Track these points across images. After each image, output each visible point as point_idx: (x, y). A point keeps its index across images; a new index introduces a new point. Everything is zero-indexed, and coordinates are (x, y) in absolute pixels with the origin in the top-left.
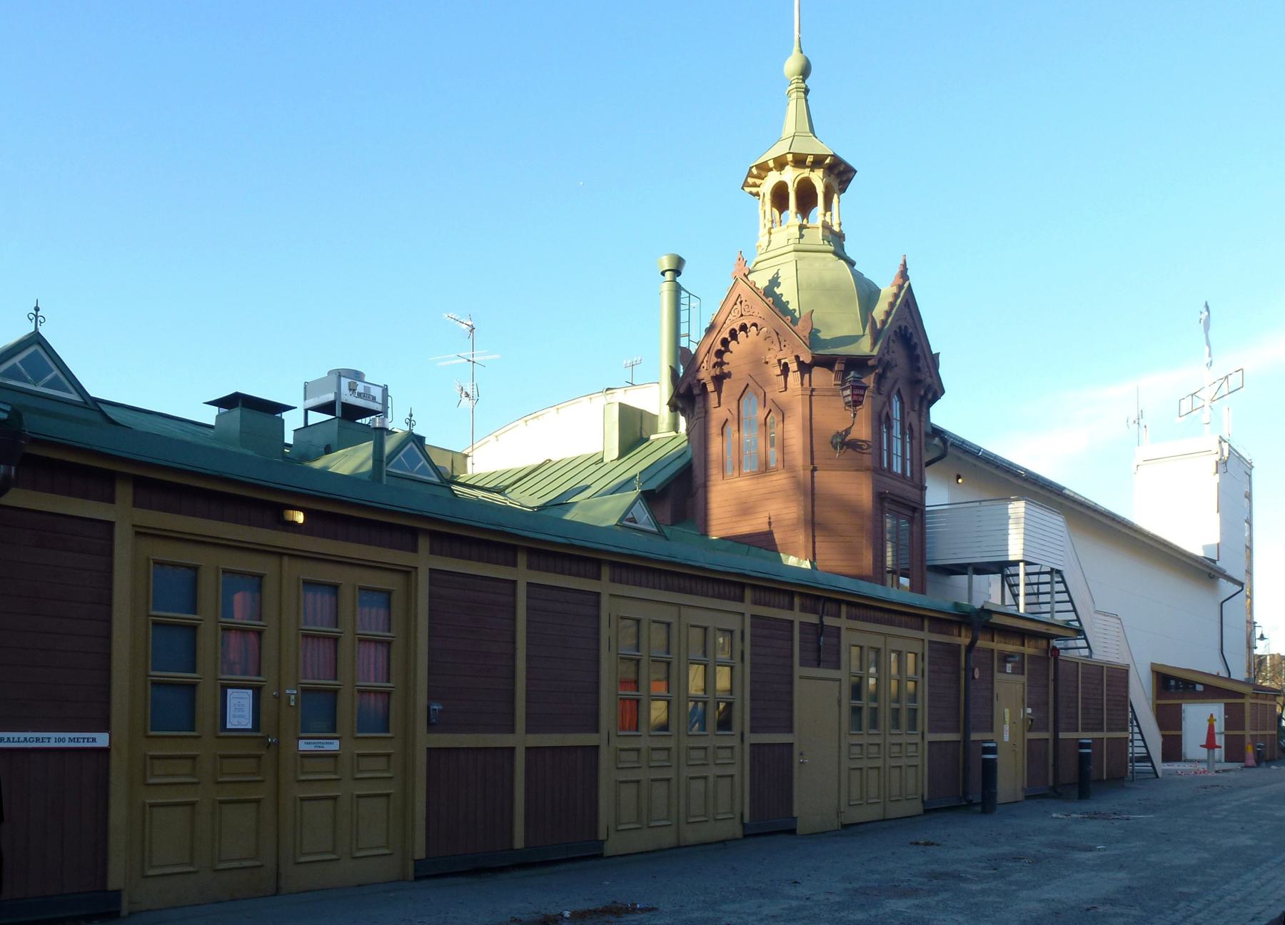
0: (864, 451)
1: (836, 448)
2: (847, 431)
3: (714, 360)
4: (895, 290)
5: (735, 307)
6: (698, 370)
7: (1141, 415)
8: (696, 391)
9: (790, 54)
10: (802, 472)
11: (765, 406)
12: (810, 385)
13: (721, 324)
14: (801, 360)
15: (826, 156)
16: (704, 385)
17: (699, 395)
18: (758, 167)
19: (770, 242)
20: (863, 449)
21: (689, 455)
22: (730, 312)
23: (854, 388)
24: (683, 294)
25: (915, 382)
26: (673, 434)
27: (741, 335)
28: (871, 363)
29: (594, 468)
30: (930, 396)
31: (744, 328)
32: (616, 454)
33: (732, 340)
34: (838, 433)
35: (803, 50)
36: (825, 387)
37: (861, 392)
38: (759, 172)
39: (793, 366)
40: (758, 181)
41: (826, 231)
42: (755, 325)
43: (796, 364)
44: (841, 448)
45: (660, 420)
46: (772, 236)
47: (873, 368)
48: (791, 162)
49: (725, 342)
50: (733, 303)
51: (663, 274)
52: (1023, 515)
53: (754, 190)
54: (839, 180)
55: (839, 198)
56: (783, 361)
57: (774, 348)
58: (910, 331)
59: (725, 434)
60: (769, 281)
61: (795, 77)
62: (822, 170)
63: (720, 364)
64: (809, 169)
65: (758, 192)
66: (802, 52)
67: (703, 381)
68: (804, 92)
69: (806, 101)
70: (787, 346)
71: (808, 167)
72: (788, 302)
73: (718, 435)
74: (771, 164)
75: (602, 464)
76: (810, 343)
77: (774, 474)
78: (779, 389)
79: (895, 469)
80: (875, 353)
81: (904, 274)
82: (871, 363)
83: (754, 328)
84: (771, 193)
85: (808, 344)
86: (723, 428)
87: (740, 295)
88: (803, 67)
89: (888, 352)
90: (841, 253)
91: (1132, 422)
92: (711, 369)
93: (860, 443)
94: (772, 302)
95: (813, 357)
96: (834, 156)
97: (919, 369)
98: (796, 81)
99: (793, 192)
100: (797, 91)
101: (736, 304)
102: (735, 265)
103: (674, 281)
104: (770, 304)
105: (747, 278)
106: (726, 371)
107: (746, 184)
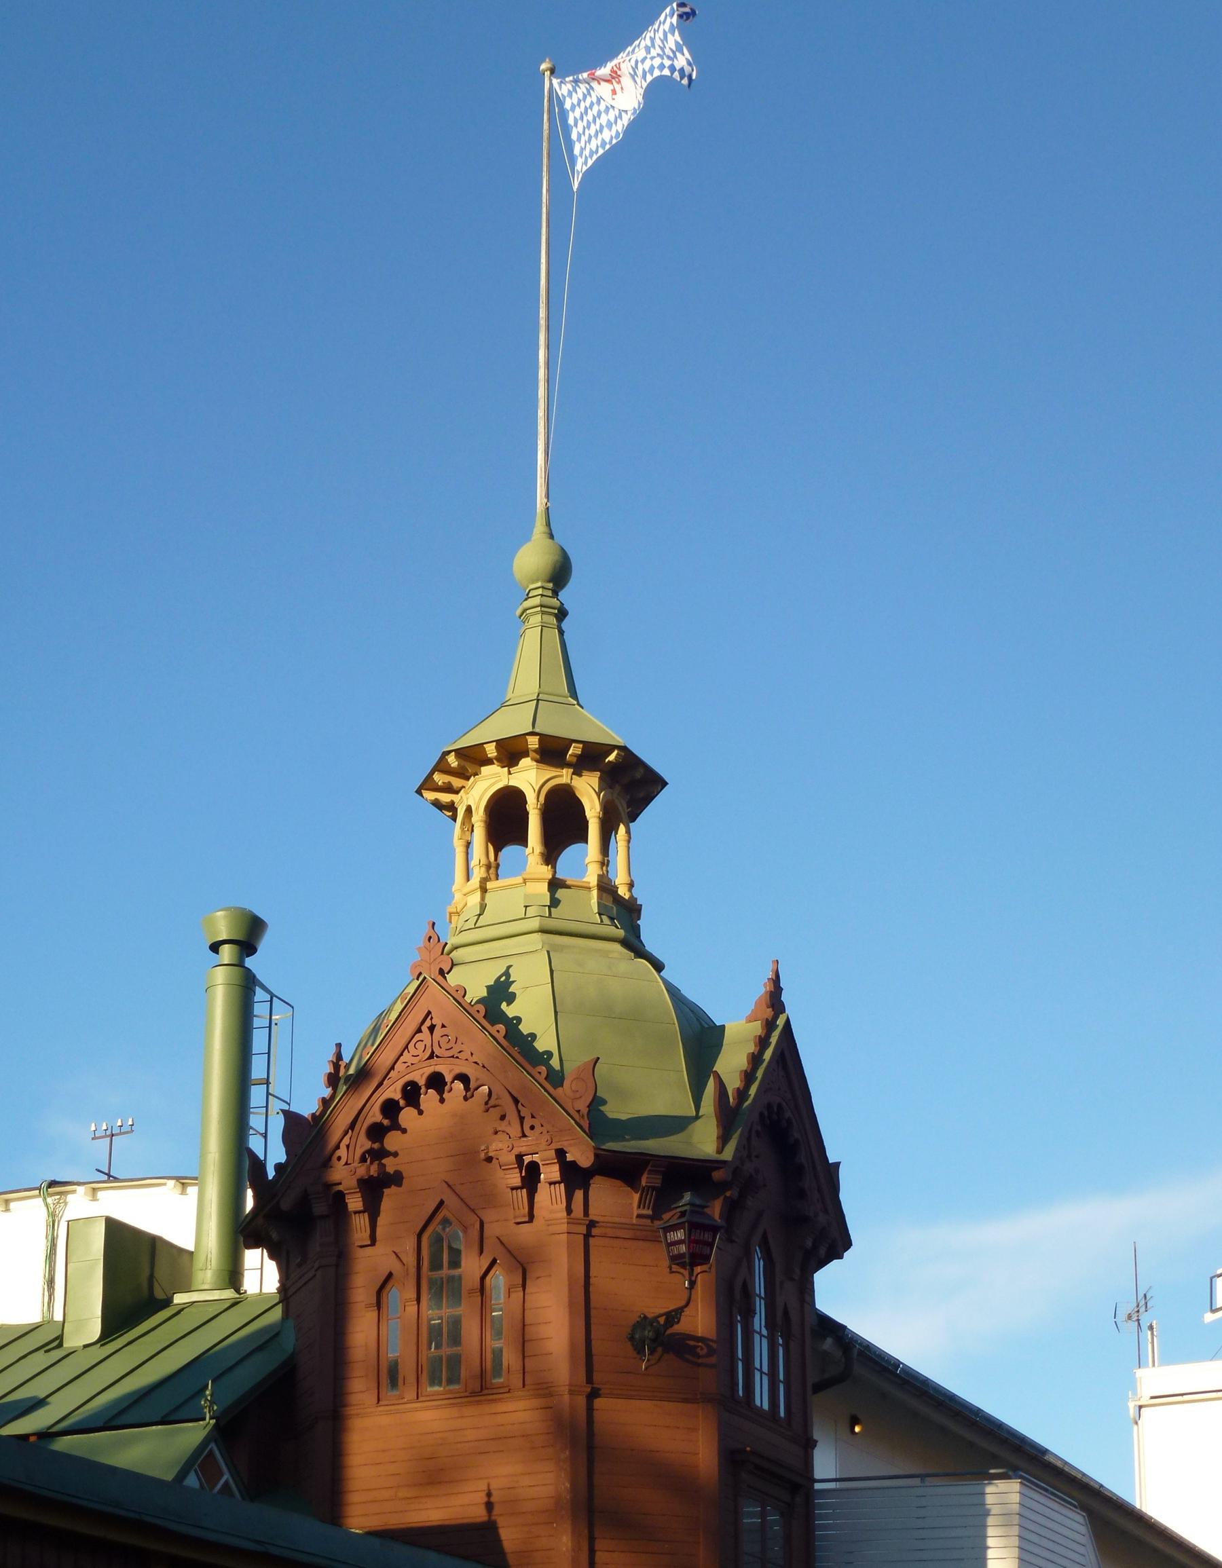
0: (700, 1361)
1: (640, 1351)
2: (673, 1317)
3: (364, 1144)
4: (757, 1028)
5: (418, 1037)
6: (327, 1163)
7: (1143, 1303)
8: (319, 1208)
9: (527, 539)
10: (566, 1397)
11: (481, 1252)
12: (586, 1212)
13: (384, 1072)
14: (569, 1157)
15: (610, 748)
16: (340, 1197)
17: (323, 1217)
18: (460, 753)
19: (483, 907)
20: (699, 1357)
21: (289, 1342)
22: (406, 1047)
23: (693, 1227)
24: (260, 995)
25: (795, 1221)
26: (229, 1294)
27: (429, 1098)
28: (717, 1175)
29: (42, 1360)
30: (822, 1251)
31: (436, 1082)
32: (95, 1329)
33: (408, 1105)
34: (645, 1317)
35: (554, 533)
36: (617, 1220)
37: (707, 1236)
38: (463, 763)
39: (550, 1172)
40: (456, 782)
41: (604, 895)
42: (463, 1078)
43: (556, 1168)
44: (652, 1352)
45: (199, 1262)
46: (488, 895)
47: (723, 1186)
48: (535, 751)
49: (390, 1109)
50: (414, 1026)
51: (215, 947)
52: (1016, 1508)
53: (445, 798)
54: (628, 797)
55: (628, 832)
56: (527, 1159)
57: (509, 1130)
58: (788, 1114)
59: (384, 1305)
60: (488, 987)
61: (539, 584)
62: (598, 774)
63: (378, 1154)
64: (571, 770)
65: (453, 803)
66: (551, 536)
67: (340, 1188)
68: (556, 616)
69: (561, 633)
70: (538, 1129)
71: (569, 765)
72: (533, 1036)
73: (368, 1306)
74: (491, 750)
75: (57, 1354)
76: (590, 1127)
77: (500, 1399)
78: (515, 1217)
79: (758, 1402)
80: (728, 1154)
81: (775, 999)
82: (717, 1175)
83: (459, 1085)
84: (487, 807)
85: (586, 1128)
86: (379, 1292)
87: (429, 1013)
88: (555, 568)
89: (749, 1156)
90: (632, 939)
91: (1125, 1317)
92: (356, 1164)
93: (692, 1343)
94: (503, 1032)
95: (596, 1156)
96: (623, 749)
97: (802, 1194)
98: (540, 591)
99: (537, 811)
100: (543, 613)
101: (419, 1031)
102: (419, 949)
103: (240, 964)
104: (500, 1037)
105: (445, 978)
106: (390, 1169)
107: (428, 784)
